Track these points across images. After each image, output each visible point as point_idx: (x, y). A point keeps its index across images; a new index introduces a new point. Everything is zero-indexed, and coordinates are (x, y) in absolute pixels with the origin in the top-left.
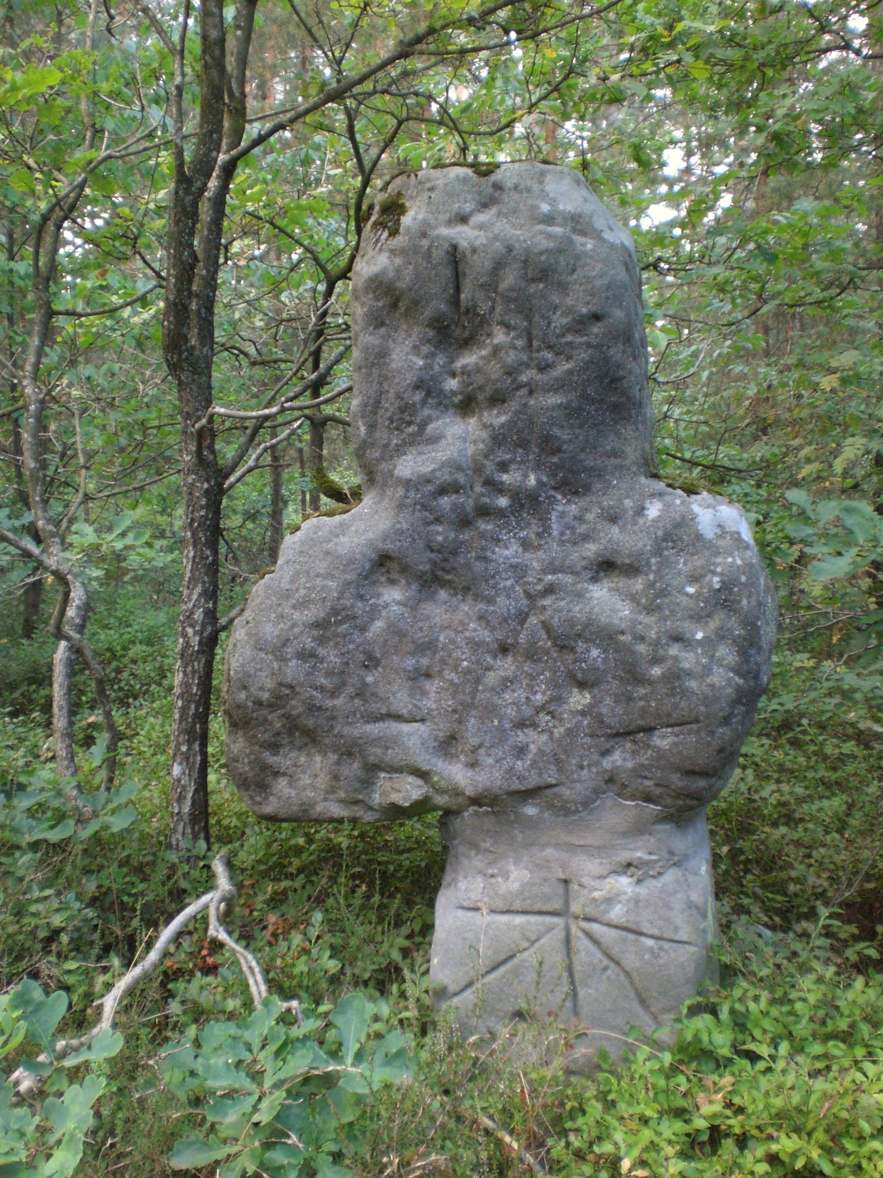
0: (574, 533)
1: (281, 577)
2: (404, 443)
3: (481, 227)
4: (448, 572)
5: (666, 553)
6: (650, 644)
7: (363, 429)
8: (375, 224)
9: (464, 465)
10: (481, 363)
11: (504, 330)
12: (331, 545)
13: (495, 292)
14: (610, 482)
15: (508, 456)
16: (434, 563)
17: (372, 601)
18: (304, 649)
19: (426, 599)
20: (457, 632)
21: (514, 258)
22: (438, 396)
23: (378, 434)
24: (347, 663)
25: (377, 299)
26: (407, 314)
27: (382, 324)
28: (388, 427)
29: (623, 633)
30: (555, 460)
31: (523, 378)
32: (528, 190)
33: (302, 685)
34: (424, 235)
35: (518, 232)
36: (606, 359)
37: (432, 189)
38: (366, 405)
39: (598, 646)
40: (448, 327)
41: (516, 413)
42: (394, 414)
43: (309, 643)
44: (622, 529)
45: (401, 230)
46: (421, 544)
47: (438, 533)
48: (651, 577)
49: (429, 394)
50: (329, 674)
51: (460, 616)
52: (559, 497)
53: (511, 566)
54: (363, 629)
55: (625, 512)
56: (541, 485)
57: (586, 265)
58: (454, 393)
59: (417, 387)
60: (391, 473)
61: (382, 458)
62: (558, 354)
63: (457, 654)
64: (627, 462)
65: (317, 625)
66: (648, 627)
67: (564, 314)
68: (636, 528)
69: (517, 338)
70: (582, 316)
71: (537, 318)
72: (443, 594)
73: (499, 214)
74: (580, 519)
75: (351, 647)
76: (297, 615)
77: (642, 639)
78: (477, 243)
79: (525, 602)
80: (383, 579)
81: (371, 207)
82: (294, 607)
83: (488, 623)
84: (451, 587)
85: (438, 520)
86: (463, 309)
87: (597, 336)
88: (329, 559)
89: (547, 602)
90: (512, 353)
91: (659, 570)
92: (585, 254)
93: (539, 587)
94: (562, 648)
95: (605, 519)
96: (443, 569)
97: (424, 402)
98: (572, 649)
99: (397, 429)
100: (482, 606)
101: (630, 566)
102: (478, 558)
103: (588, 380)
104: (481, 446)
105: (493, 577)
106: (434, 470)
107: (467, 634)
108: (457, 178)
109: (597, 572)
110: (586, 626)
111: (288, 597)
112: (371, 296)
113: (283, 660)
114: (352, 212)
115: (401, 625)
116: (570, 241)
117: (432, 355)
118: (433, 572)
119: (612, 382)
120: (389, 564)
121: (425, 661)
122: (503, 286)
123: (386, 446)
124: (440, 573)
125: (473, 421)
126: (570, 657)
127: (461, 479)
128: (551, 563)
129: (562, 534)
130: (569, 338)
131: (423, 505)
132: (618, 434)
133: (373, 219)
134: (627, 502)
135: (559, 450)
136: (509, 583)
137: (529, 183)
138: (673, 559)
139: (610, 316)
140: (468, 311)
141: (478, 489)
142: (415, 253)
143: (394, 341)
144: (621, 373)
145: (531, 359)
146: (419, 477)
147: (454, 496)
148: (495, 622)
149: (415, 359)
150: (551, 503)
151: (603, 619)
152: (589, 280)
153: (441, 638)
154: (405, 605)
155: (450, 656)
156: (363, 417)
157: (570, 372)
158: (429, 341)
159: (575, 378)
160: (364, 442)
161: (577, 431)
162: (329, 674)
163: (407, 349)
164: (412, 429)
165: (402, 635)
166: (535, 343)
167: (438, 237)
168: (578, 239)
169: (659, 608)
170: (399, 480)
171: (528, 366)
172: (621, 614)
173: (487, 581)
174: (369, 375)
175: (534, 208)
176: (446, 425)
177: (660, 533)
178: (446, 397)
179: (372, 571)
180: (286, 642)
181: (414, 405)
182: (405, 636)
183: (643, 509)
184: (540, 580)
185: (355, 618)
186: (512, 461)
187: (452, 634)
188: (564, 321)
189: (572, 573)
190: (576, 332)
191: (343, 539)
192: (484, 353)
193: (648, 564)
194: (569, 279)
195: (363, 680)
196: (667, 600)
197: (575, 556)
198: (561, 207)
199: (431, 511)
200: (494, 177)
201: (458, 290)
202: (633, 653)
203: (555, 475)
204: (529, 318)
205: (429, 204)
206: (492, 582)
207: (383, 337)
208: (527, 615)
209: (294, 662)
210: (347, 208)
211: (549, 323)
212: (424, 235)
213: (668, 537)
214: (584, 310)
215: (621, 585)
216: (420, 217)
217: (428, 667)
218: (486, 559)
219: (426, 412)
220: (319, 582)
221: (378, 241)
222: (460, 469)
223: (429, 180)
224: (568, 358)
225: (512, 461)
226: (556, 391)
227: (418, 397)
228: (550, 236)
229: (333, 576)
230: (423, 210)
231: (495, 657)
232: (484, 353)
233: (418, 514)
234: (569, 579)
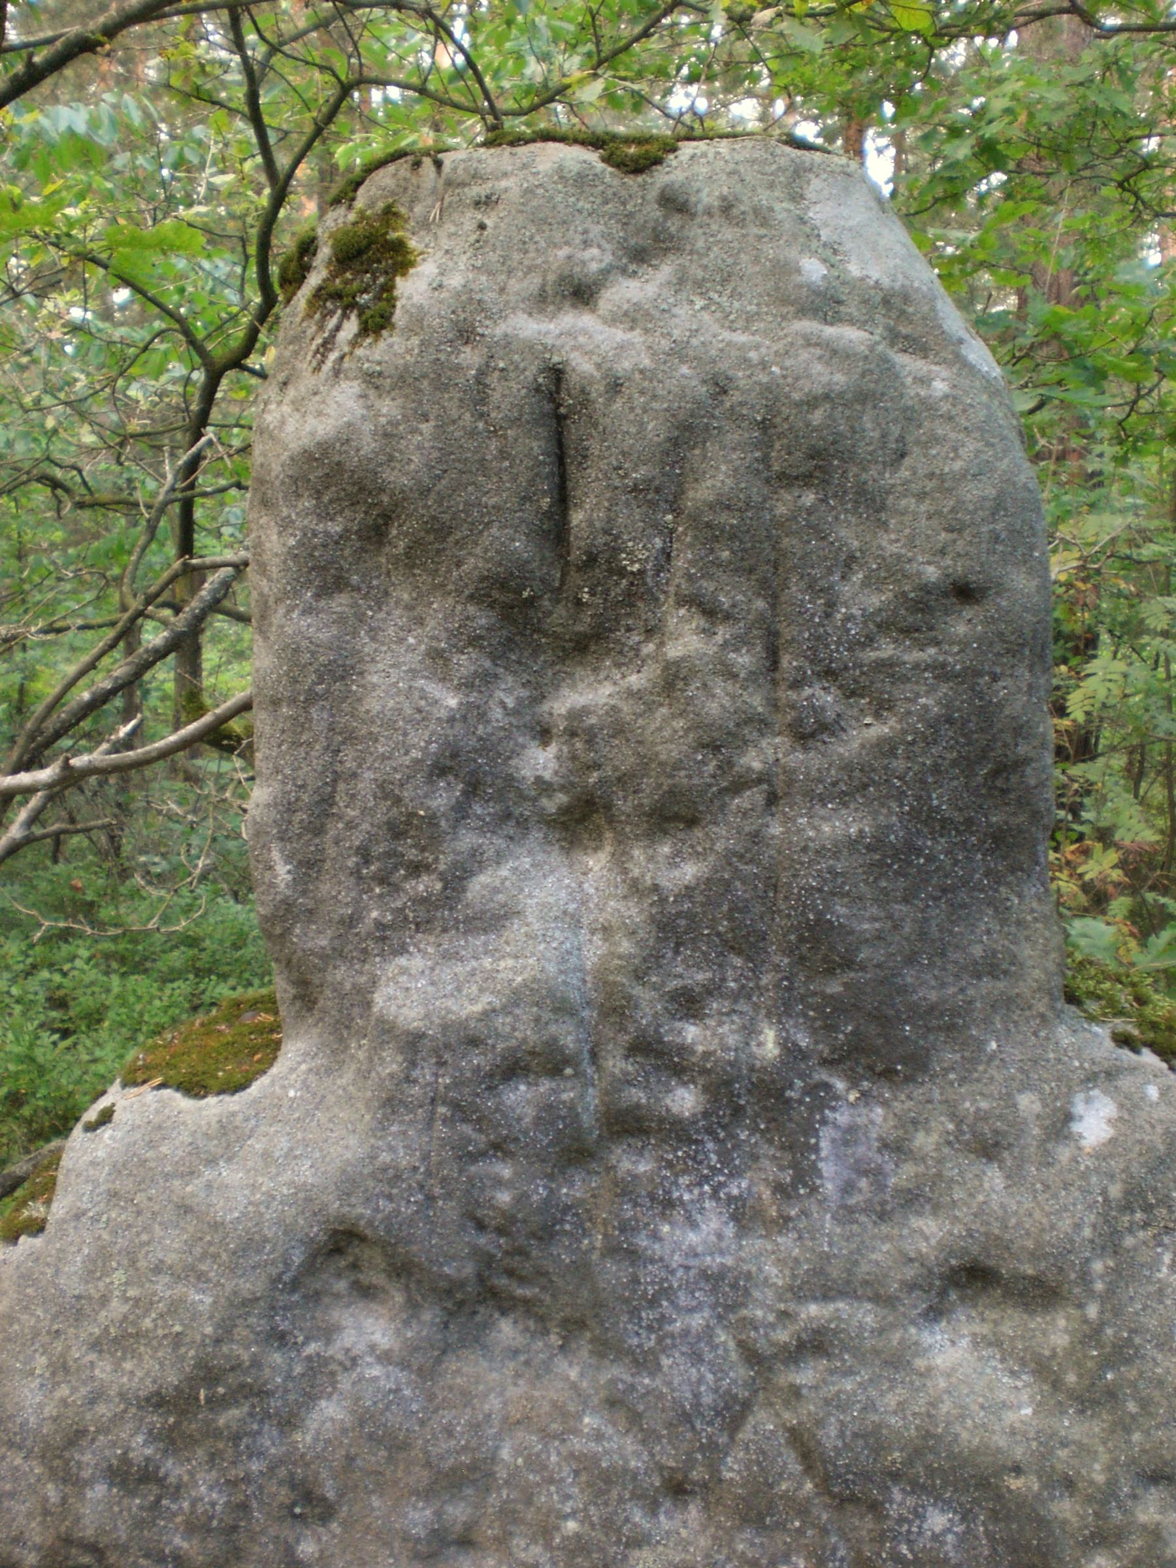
0: (880, 1187)
1: (61, 1258)
2: (401, 920)
3: (632, 317)
4: (522, 1280)
5: (1129, 1241)
6: (1089, 1499)
7: (283, 872)
8: (321, 295)
9: (574, 996)
10: (627, 708)
11: (699, 621)
12: (193, 1187)
13: (677, 511)
14: (981, 1044)
15: (701, 977)
16: (486, 1260)
17: (312, 1348)
18: (124, 1459)
19: (463, 1343)
20: (546, 1436)
21: (733, 415)
22: (500, 796)
23: (325, 888)
24: (244, 1507)
25: (325, 515)
26: (410, 560)
27: (339, 584)
28: (356, 873)
29: (1017, 1470)
30: (834, 988)
31: (753, 761)
32: (763, 216)
33: (124, 1549)
34: (466, 334)
35: (741, 338)
36: (987, 713)
37: (486, 203)
38: (291, 808)
39: (946, 1505)
40: (531, 602)
41: (729, 856)
42: (372, 838)
43: (141, 1448)
44: (1014, 1177)
45: (399, 317)
46: (449, 1209)
47: (499, 1183)
48: (1092, 1311)
49: (473, 788)
50: (196, 1527)
51: (551, 1392)
52: (840, 1085)
53: (704, 1275)
54: (289, 1422)
55: (1019, 1125)
56: (790, 1049)
57: (935, 440)
58: (544, 787)
59: (440, 770)
60: (363, 998)
61: (338, 953)
62: (851, 694)
63: (549, 1497)
64: (1023, 988)
65: (158, 1401)
66: (1084, 1451)
67: (872, 582)
68: (1049, 1174)
69: (737, 643)
70: (925, 589)
71: (795, 590)
72: (507, 1330)
73: (681, 281)
74: (897, 1148)
75: (255, 1466)
76: (103, 1370)
77: (1069, 1484)
78: (625, 365)
79: (741, 1373)
80: (341, 1286)
81: (307, 247)
82: (95, 1345)
83: (635, 1418)
84: (528, 1313)
85: (499, 1148)
86: (576, 555)
87: (964, 645)
88: (191, 1225)
89: (805, 1375)
90: (720, 687)
91: (1111, 1291)
92: (928, 405)
93: (783, 1336)
94: (843, 1502)
95: (968, 1148)
96: (511, 1273)
97: (461, 812)
98: (875, 1508)
99: (382, 881)
100: (619, 1372)
101: (1037, 1281)
102: (612, 1250)
103: (936, 769)
104: (626, 946)
105: (653, 1303)
106: (488, 1014)
107: (576, 1444)
108: (560, 173)
109: (943, 1293)
110: (916, 1453)
111: (79, 1316)
112: (307, 503)
113: (70, 1479)
114: (252, 250)
115: (394, 1418)
116: (888, 368)
117: (483, 681)
118: (481, 1278)
119: (995, 773)
120: (355, 1250)
121: (458, 1512)
122: (700, 494)
123: (350, 922)
124: (502, 1282)
125: (597, 862)
126: (865, 1525)
127: (569, 1037)
128: (818, 1272)
129: (848, 1188)
130: (886, 650)
131: (456, 1106)
132: (1001, 911)
133: (314, 280)
134: (1028, 1103)
135: (848, 963)
136: (697, 1321)
137: (764, 197)
138: (1144, 1256)
139: (1001, 589)
140: (592, 560)
141: (616, 1064)
142: (441, 386)
143: (373, 633)
144: (1022, 749)
145: (774, 705)
146: (445, 1027)
147: (545, 1085)
148: (655, 1420)
149: (434, 689)
150: (822, 1105)
151: (967, 1437)
152: (944, 484)
153: (505, 1453)
154: (404, 1365)
155: (529, 1502)
156: (282, 838)
157: (886, 748)
158: (474, 641)
159: (899, 764)
160: (287, 905)
161: (899, 909)
162: (196, 1527)
163: (413, 660)
164: (424, 885)
165: (396, 1445)
166: (788, 662)
167: (507, 342)
168: (908, 364)
169: (1112, 1394)
170: (387, 1030)
171: (763, 725)
172: (1010, 1417)
173: (634, 1313)
174: (299, 725)
175: (784, 269)
176: (522, 876)
177: (1115, 1191)
178: (522, 797)
179: (310, 1267)
180: (76, 1437)
181: (432, 820)
182: (405, 1446)
183: (1069, 1117)
184: (784, 1315)
185: (262, 1393)
186: (713, 990)
187: (533, 1440)
188: (874, 601)
189: (876, 1299)
190: (906, 631)
191: (229, 1174)
192: (635, 680)
193: (1085, 1277)
194: (889, 479)
195: (289, 1551)
196: (1131, 1373)
197: (882, 1253)
198: (854, 270)
199: (481, 1122)
200: (661, 177)
201: (563, 499)
202: (1042, 1523)
203: (831, 1028)
204: (772, 592)
205: (478, 246)
206: (648, 1315)
207: (341, 620)
208: (747, 1406)
209: (99, 1491)
210: (244, 241)
211: (831, 605)
212: (466, 334)
213: (1134, 1198)
214: (932, 573)
215: (1007, 1329)
216: (455, 281)
217: (469, 1527)
218: (633, 1255)
219: (467, 840)
220: (162, 1287)
221: (328, 344)
222: (563, 1008)
223: (476, 177)
224: (882, 707)
225: (713, 990)
226: (844, 799)
227: (443, 798)
228: (834, 353)
229: (201, 1276)
230: (463, 261)
231: (653, 1509)
232: (635, 680)
233: (442, 1131)
234: (866, 1316)
